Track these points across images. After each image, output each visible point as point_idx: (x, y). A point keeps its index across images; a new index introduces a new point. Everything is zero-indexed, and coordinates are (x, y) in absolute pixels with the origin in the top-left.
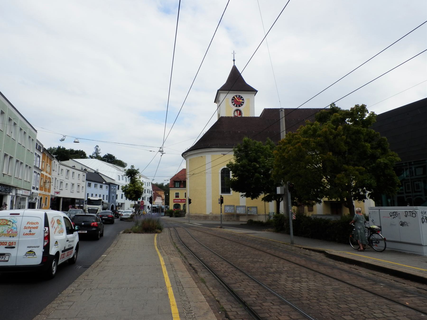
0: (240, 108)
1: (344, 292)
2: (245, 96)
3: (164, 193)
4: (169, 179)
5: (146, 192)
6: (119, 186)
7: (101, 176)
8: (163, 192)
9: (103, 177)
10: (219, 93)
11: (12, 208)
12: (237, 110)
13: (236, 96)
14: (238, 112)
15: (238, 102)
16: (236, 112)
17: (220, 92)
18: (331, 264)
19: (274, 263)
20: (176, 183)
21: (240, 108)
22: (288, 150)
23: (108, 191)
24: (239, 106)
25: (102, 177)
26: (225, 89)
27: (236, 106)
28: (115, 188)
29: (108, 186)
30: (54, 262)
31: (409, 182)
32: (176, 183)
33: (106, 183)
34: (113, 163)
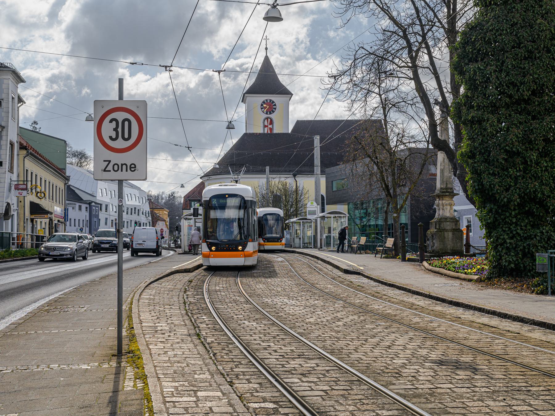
0: (270, 116)
2: (277, 99)
3: (167, 213)
5: (140, 214)
6: (101, 205)
7: (74, 191)
8: (166, 211)
9: (77, 191)
10: (245, 97)
12: (267, 118)
13: (267, 100)
14: (269, 120)
15: (270, 108)
16: (266, 120)
17: (246, 95)
18: (549, 369)
19: (398, 357)
20: (193, 203)
21: (270, 116)
22: (437, 103)
23: (88, 214)
24: (270, 113)
25: (75, 193)
26: (253, 90)
27: (267, 113)
28: (97, 208)
30: (258, 210)
32: (193, 203)
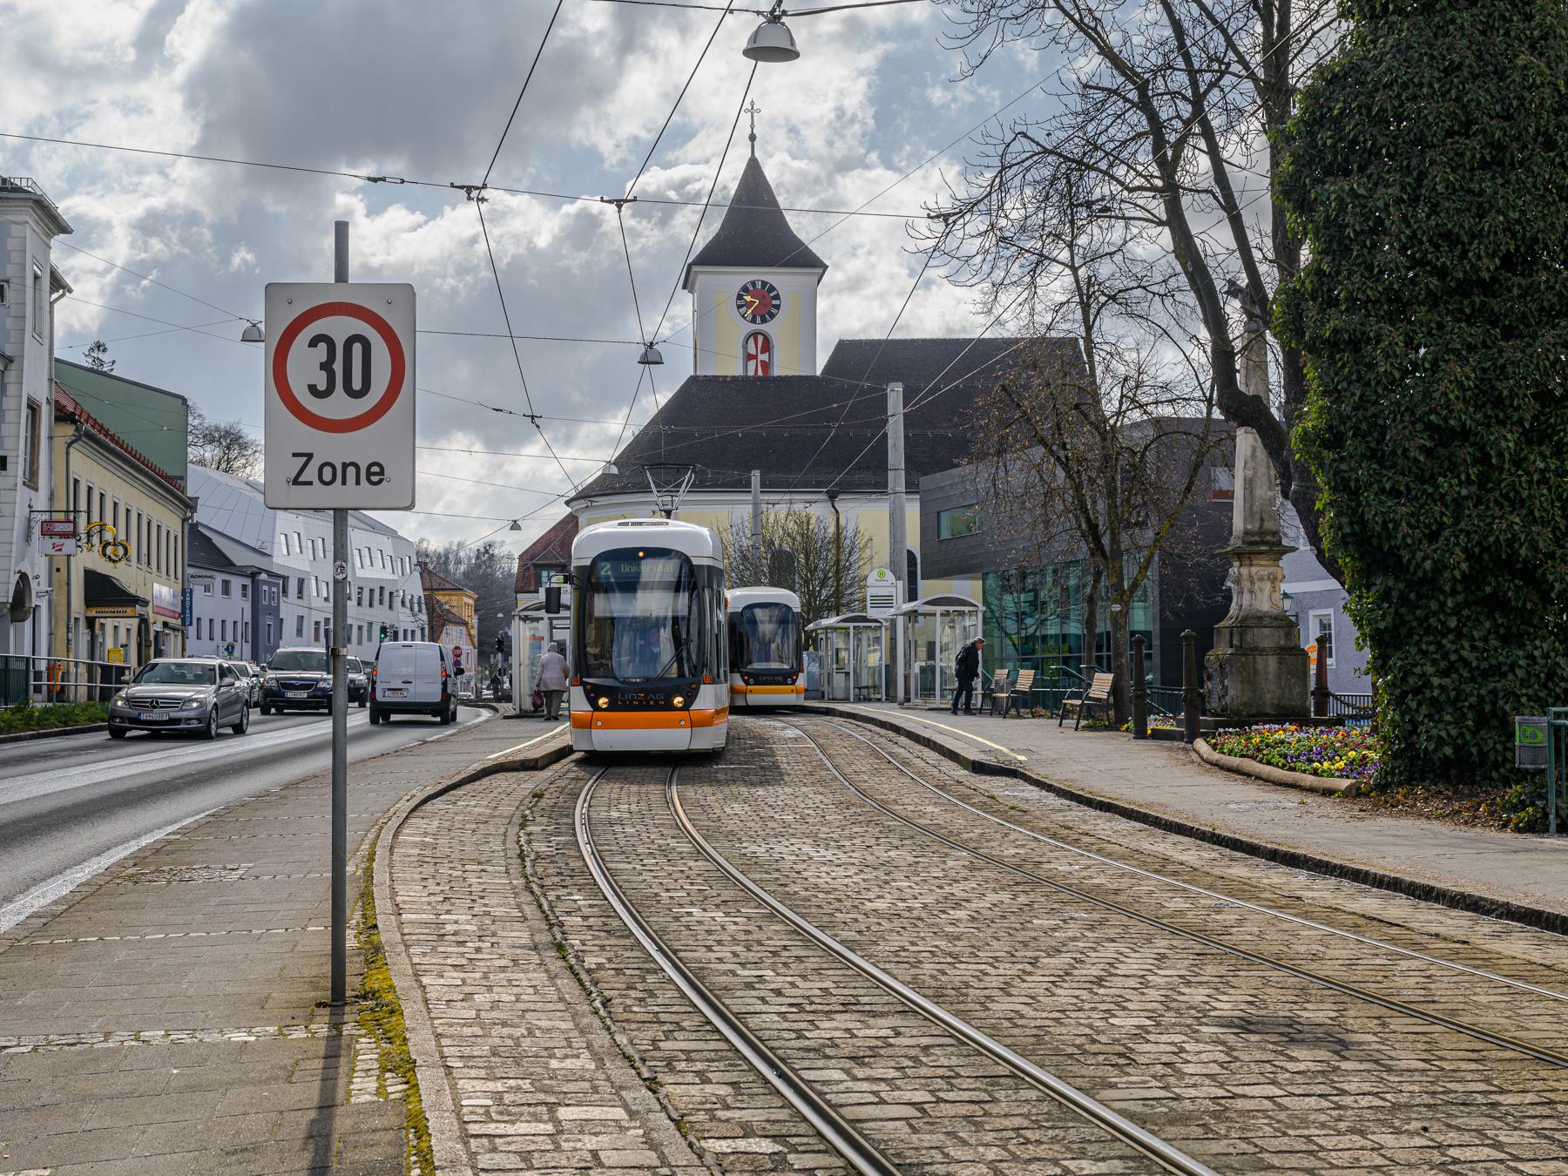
0: (763, 327)
1: (1517, 1159)
2: (781, 279)
3: (471, 602)
4: (516, 555)
5: (395, 604)
6: (285, 579)
7: (209, 540)
8: (470, 597)
9: (217, 540)
10: (692, 274)
11: (405, 639)
12: (755, 335)
14: (760, 339)
15: (764, 304)
16: (751, 340)
17: (695, 268)
20: (544, 574)
21: (763, 327)
22: (1234, 290)
23: (248, 606)
24: (764, 321)
25: (213, 545)
26: (715, 256)
27: (753, 321)
28: (274, 589)
29: (248, 582)
31: (405, 639)
32: (544, 574)
33: (240, 572)
34: (628, 622)
